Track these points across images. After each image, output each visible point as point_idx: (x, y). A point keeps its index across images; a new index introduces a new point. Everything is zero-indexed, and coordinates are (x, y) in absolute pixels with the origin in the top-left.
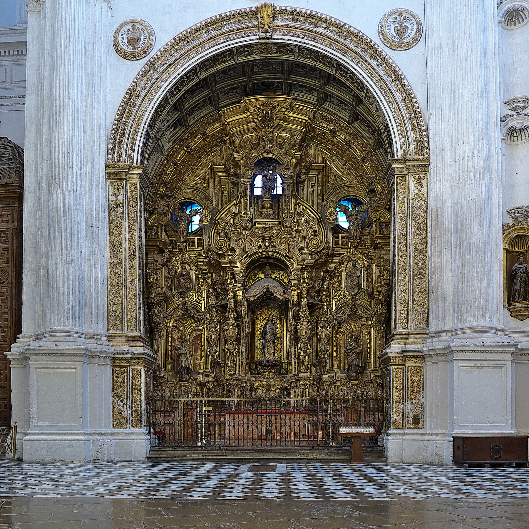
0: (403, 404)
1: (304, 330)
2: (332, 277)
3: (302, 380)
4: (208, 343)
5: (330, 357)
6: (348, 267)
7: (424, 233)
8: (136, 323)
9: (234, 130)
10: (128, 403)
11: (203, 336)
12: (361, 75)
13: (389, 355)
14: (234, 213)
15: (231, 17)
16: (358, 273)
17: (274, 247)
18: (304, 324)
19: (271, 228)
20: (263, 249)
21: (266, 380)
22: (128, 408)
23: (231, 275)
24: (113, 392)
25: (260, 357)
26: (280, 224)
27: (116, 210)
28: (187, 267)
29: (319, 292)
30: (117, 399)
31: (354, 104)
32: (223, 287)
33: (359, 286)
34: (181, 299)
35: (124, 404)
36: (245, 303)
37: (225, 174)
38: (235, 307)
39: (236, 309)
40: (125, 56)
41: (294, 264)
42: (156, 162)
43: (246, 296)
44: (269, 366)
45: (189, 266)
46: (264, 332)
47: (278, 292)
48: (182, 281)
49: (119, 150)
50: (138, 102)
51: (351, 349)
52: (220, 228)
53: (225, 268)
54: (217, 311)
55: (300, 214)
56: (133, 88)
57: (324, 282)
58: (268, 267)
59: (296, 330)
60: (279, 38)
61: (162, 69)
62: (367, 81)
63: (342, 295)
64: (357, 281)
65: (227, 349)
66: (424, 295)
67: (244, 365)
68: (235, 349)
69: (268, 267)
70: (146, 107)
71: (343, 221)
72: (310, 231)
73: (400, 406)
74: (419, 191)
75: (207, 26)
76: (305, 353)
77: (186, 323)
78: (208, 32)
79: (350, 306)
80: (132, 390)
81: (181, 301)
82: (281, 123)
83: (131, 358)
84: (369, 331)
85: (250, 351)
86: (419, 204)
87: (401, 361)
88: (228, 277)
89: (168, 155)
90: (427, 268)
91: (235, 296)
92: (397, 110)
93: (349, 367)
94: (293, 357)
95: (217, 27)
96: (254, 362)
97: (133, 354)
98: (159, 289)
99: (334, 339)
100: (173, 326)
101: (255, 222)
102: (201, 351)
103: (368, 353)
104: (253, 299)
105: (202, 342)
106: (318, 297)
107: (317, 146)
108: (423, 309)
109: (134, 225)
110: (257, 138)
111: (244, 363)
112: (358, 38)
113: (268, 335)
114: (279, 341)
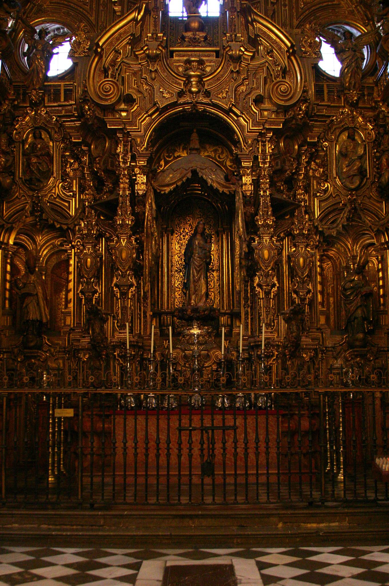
1: (265, 245)
2: (312, 157)
4: (80, 275)
6: (340, 140)
11: (72, 262)
14: (132, 35)
16: (361, 151)
17: (207, 94)
18: (266, 239)
20: (187, 98)
23: (125, 146)
26: (217, 57)
29: (291, 183)
32: (109, 167)
33: (362, 172)
36: (150, 200)
38: (133, 204)
41: (243, 125)
43: (155, 185)
45: (49, 133)
46: (188, 255)
47: (214, 179)
48: (34, 160)
51: (352, 288)
52: (108, 60)
55: (253, 42)
57: (299, 164)
58: (195, 136)
59: (251, 250)
65: (116, 286)
68: (132, 285)
69: (195, 136)
71: (330, 64)
76: (267, 293)
77: (39, 239)
79: (347, 210)
81: (31, 197)
88: (120, 149)
91: (132, 183)
93: (349, 321)
94: (243, 302)
96: (167, 314)
100: (15, 244)
101: (172, 52)
102: (68, 291)
103: (380, 297)
104: (167, 190)
105: (69, 273)
111: (149, 313)
113: (196, 260)
114: (215, 274)
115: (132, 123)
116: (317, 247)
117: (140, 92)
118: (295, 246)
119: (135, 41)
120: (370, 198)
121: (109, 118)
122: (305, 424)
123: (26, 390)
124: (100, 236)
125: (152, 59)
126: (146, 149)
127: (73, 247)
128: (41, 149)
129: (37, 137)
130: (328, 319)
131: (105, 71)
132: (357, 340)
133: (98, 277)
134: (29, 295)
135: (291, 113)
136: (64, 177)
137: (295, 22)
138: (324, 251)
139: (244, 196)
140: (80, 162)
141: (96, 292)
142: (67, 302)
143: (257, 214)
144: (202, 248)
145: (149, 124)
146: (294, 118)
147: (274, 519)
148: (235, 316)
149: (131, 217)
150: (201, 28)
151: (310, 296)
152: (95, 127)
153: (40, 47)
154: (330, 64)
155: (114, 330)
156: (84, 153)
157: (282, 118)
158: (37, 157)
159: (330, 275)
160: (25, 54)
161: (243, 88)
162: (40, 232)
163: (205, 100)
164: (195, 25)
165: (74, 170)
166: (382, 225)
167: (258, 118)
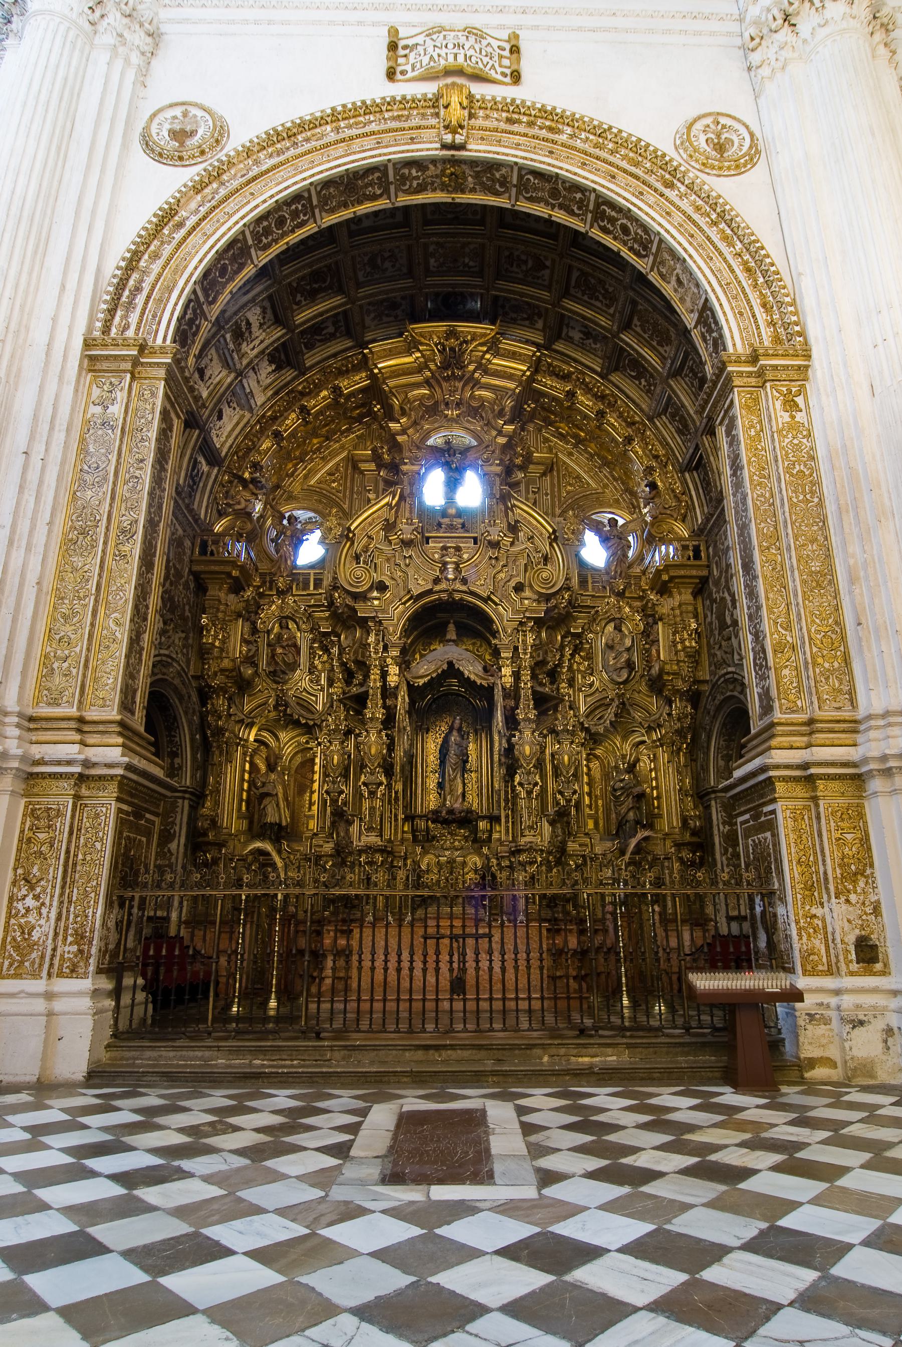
0: (822, 904)
1: (527, 743)
2: (576, 650)
3: (525, 851)
5: (578, 805)
7: (816, 500)
8: (113, 689)
9: (392, 383)
10: (55, 903)
11: (317, 760)
12: (647, 214)
13: (771, 773)
15: (384, 108)
18: (527, 734)
20: (443, 586)
21: (447, 853)
22: (53, 915)
23: (376, 635)
24: (15, 869)
26: (475, 543)
27: (100, 432)
28: (291, 625)
29: (553, 675)
30: (24, 891)
31: (615, 328)
32: (360, 658)
33: (630, 665)
34: (275, 686)
35: (43, 904)
36: (403, 693)
37: (373, 466)
38: (384, 697)
39: (384, 702)
40: (160, 156)
41: (504, 615)
42: (237, 424)
43: (408, 676)
44: (454, 821)
47: (472, 670)
48: (279, 651)
49: (125, 317)
50: (178, 236)
51: (622, 788)
52: (358, 547)
53: (365, 620)
54: (348, 712)
56: (171, 209)
57: (562, 656)
60: (478, 149)
61: (235, 184)
62: (660, 224)
63: (597, 684)
64: (625, 656)
65: (364, 784)
66: (833, 632)
67: (400, 822)
68: (381, 784)
73: (814, 911)
74: (793, 417)
75: (334, 117)
76: (529, 793)
78: (337, 130)
79: (615, 704)
80: (75, 865)
81: (275, 690)
82: (476, 375)
83: (80, 774)
84: (654, 755)
85: (413, 794)
86: (796, 441)
87: (800, 791)
88: (371, 639)
89: (263, 416)
90: (832, 571)
91: (384, 675)
92: (726, 273)
93: (621, 825)
94: (503, 804)
95: (357, 123)
97: (87, 764)
98: (226, 661)
99: (585, 769)
100: (255, 741)
101: (428, 538)
102: (312, 792)
104: (421, 682)
105: (313, 772)
106: (552, 683)
107: (540, 430)
108: (836, 665)
109: (141, 469)
110: (431, 396)
111: (401, 816)
112: (638, 149)
113: (452, 758)
114: (473, 775)
116: (583, 745)
120: (639, 692)
122: (573, 942)
124: (348, 733)
128: (288, 639)
129: (284, 627)
130: (596, 824)
131: (357, 558)
133: (346, 776)
134: (268, 795)
135: (553, 602)
136: (312, 669)
137: (558, 511)
139: (504, 689)
141: (342, 792)
142: (311, 804)
146: (555, 607)
147: (538, 1051)
148: (494, 819)
149: (382, 711)
152: (346, 615)
157: (543, 607)
158: (283, 647)
159: (597, 773)
161: (502, 575)
162: (285, 727)
163: (464, 588)
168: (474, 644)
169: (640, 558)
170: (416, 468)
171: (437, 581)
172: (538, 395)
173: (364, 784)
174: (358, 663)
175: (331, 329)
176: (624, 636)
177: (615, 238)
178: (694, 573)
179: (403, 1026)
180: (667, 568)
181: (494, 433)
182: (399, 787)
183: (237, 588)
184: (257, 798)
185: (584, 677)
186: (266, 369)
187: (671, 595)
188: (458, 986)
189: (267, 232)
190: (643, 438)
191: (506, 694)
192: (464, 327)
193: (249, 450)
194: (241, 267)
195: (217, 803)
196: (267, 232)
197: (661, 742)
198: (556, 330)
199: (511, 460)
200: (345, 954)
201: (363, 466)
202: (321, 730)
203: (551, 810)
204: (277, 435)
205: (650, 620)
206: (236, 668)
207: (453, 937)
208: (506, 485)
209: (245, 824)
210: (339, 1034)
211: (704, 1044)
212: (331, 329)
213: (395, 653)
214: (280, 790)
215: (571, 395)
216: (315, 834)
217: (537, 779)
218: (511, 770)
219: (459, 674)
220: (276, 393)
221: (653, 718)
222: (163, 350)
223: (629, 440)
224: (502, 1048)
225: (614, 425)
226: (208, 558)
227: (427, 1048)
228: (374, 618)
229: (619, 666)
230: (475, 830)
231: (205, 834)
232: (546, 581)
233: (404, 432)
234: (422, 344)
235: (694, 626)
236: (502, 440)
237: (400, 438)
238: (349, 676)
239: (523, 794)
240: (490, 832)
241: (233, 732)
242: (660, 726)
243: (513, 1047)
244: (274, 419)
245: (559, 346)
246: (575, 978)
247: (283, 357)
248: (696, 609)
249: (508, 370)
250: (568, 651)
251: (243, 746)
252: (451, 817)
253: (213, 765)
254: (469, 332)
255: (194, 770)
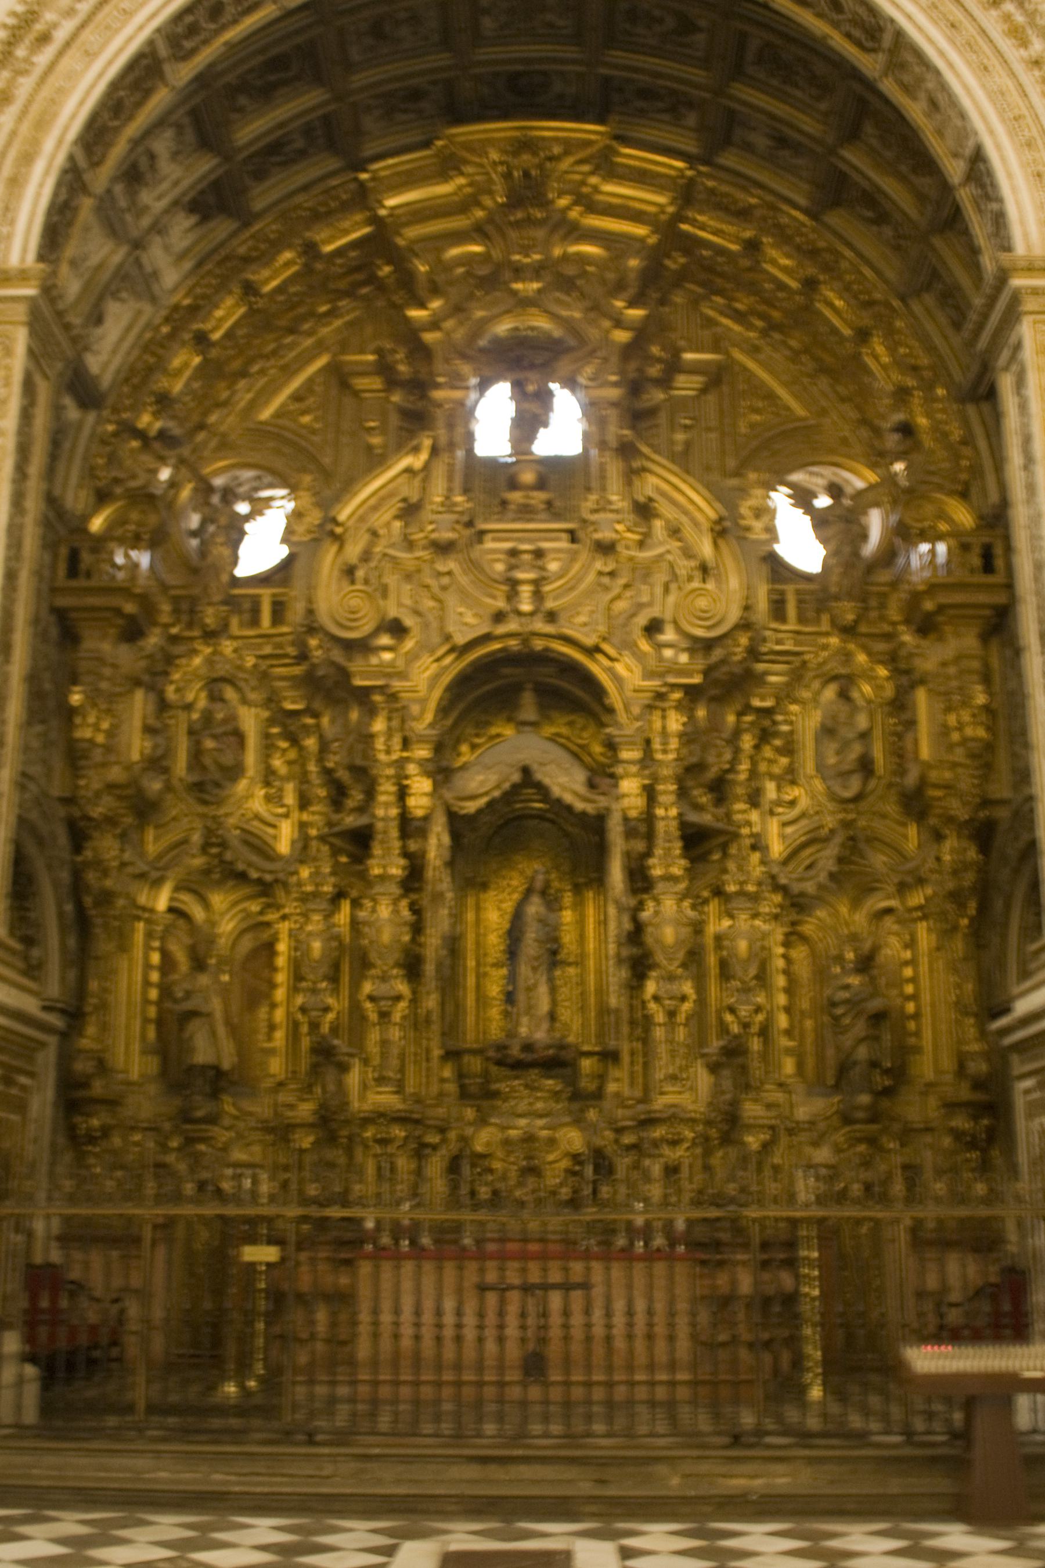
1: (667, 916)
2: (764, 736)
4: (297, 976)
5: (765, 1032)
9: (412, 232)
11: (282, 947)
14: (404, 500)
18: (669, 905)
19: (539, 554)
21: (523, 1122)
25: (495, 1030)
28: (230, 693)
29: (720, 789)
32: (358, 762)
33: (866, 766)
41: (624, 676)
46: (514, 935)
47: (566, 782)
48: (209, 744)
51: (846, 1002)
52: (353, 551)
53: (367, 691)
55: (644, 511)
57: (737, 751)
58: (528, 698)
68: (398, 998)
69: (528, 698)
70: (73, 77)
71: (801, 546)
72: (685, 567)
76: (672, 1014)
79: (838, 839)
81: (203, 816)
88: (379, 725)
91: (402, 793)
92: (1015, 97)
93: (843, 1069)
96: (474, 1052)
99: (780, 963)
100: (171, 910)
101: (482, 533)
102: (273, 1006)
111: (437, 1052)
113: (530, 946)
115: (402, 675)
116: (776, 917)
117: (417, 613)
118: (732, 917)
119: (410, 511)
120: (884, 816)
121: (356, 665)
122: (746, 1284)
123: (188, 1210)
124: (339, 895)
125: (443, 549)
126: (432, 725)
127: (284, 918)
128: (225, 721)
129: (215, 697)
130: (800, 1066)
131: (349, 572)
132: (858, 1108)
133: (334, 978)
134: (194, 1014)
135: (718, 654)
136: (268, 776)
137: (731, 463)
138: (793, 924)
139: (626, 819)
140: (301, 749)
141: (327, 1009)
142: (272, 1027)
143: (648, 854)
144: (542, 921)
145: (436, 677)
146: (723, 662)
147: (662, 1469)
148: (609, 1057)
149: (402, 862)
150: (541, 484)
151: (760, 1017)
152: (331, 683)
153: (223, 520)
154: (801, 546)
155: (364, 1086)
156: (306, 729)
157: (701, 664)
158: (215, 737)
159: (803, 971)
160: (194, 534)
161: (621, 605)
162: (219, 884)
163: (549, 629)
164: (528, 477)
165: (290, 763)
166: (910, 872)
167: (652, 663)
168: (571, 724)
169: (888, 555)
170: (457, 394)
171: (499, 617)
172: (690, 245)
173: (372, 998)
174: (353, 769)
175: (299, 144)
176: (855, 709)
177: (820, 15)
178: (982, 598)
179: (446, 1427)
180: (933, 588)
181: (607, 324)
182: (431, 1002)
183: (132, 632)
184: (173, 1021)
185: (779, 788)
186: (182, 230)
187: (941, 639)
188: (534, 1365)
189: (193, 30)
190: (890, 333)
191: (630, 833)
192: (552, 129)
193: (150, 370)
194: (148, 93)
195: (104, 1027)
196: (193, 30)
197: (924, 913)
198: (721, 132)
199: (640, 370)
200: (342, 1299)
201: (361, 383)
202: (288, 892)
203: (715, 1044)
204: (201, 340)
205: (904, 680)
206: (134, 783)
207: (527, 1289)
208: (633, 422)
209: (153, 1065)
210: (342, 1438)
211: (934, 1460)
212: (299, 144)
213: (423, 752)
214: (216, 1005)
215: (752, 246)
216: (281, 1084)
217: (688, 988)
218: (640, 966)
219: (542, 789)
220: (199, 264)
221: (910, 866)
222: (23, 276)
223: (863, 335)
224: (604, 1463)
225: (835, 306)
226: (82, 582)
227: (484, 1460)
228: (381, 687)
229: (846, 767)
230: (572, 1080)
231: (85, 1085)
232: (702, 616)
233: (434, 325)
234: (466, 162)
235: (981, 699)
236: (622, 336)
237: (430, 337)
238: (338, 794)
239: (660, 1017)
240: (602, 1078)
241: (128, 896)
242: (921, 881)
243: (624, 1461)
244: (194, 310)
245: (729, 159)
246: (751, 1345)
247: (210, 203)
248: (986, 665)
249: (632, 204)
250: (747, 742)
251: (148, 921)
252: (528, 1057)
253: (97, 958)
254: (556, 140)
255: (65, 965)
